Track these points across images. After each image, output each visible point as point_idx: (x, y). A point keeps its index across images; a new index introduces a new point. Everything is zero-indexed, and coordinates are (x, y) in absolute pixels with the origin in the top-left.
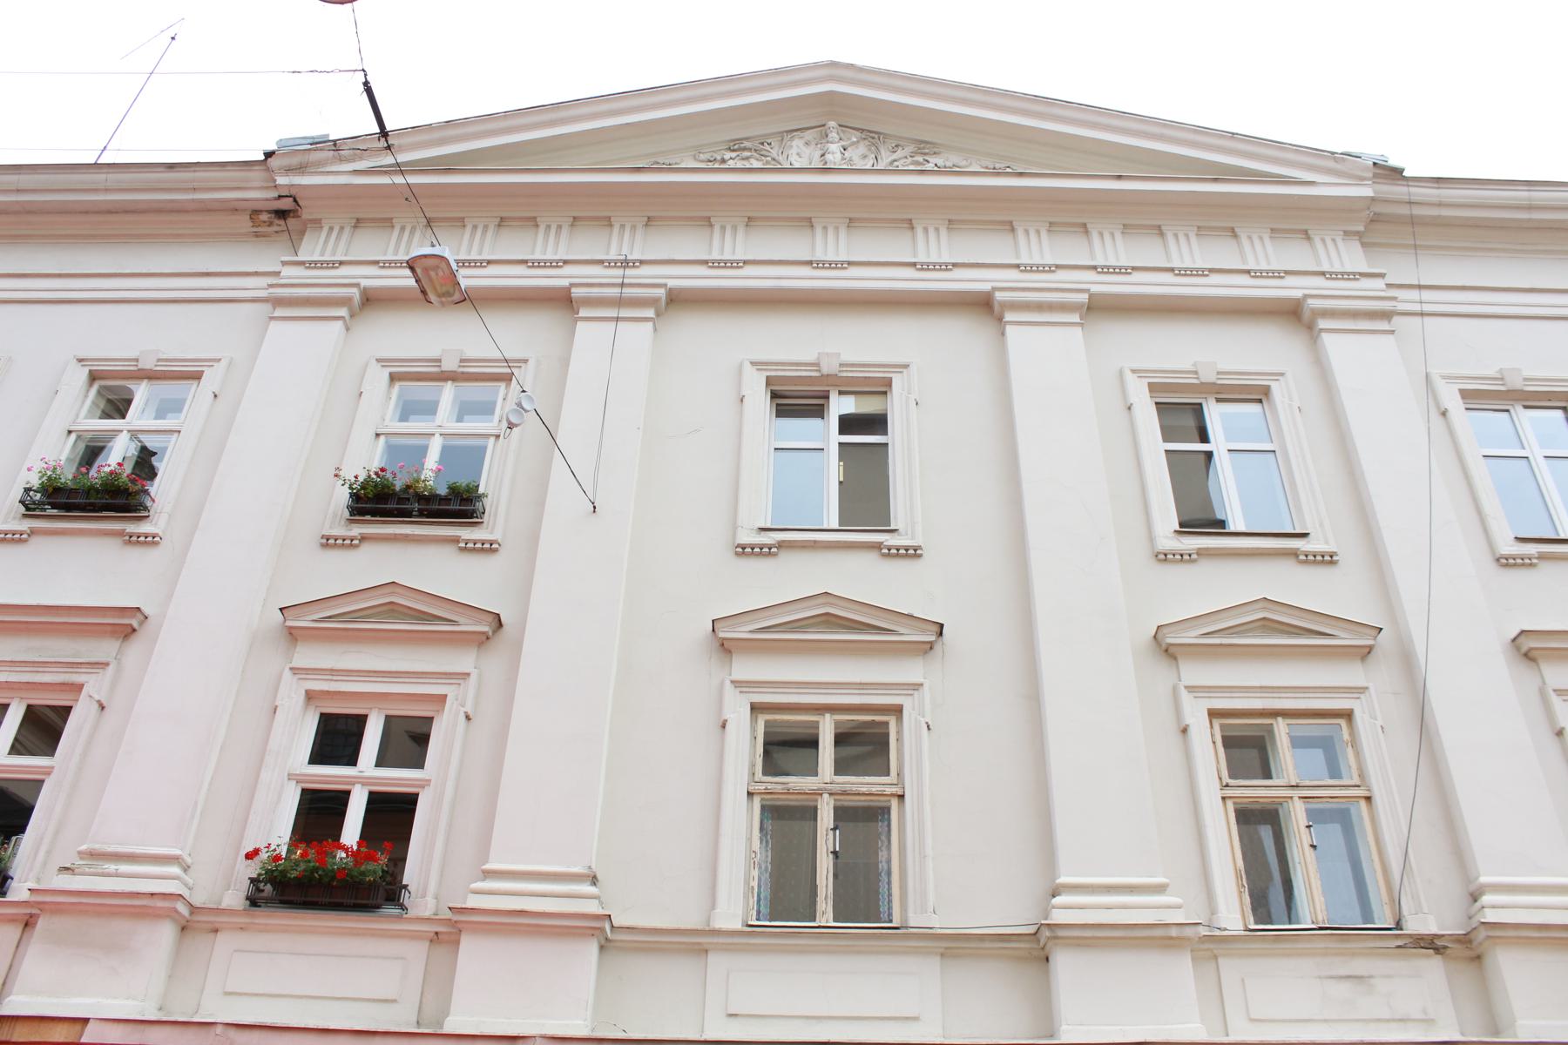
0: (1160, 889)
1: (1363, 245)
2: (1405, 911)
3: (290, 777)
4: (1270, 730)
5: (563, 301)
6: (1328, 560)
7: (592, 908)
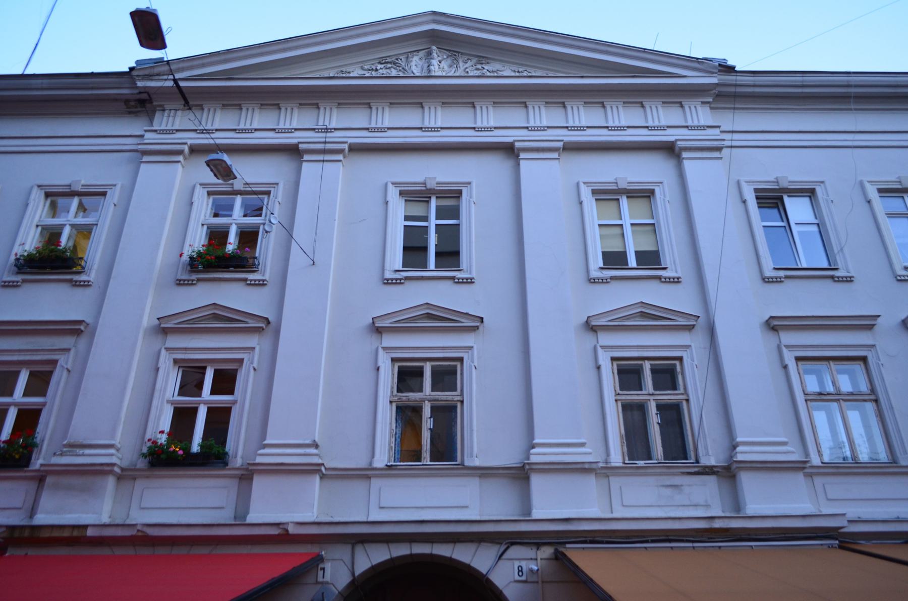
0: (582, 445)
1: (711, 108)
3: (168, 402)
4: (641, 365)
5: (294, 152)
6: (676, 281)
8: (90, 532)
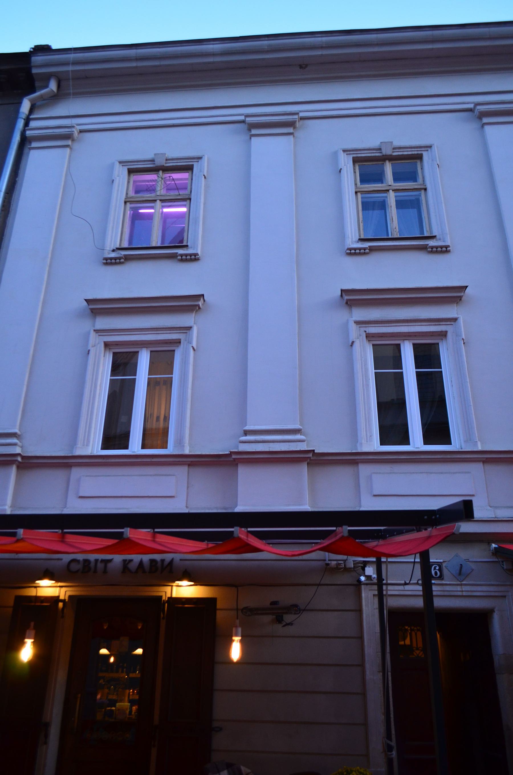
7: (303, 447)
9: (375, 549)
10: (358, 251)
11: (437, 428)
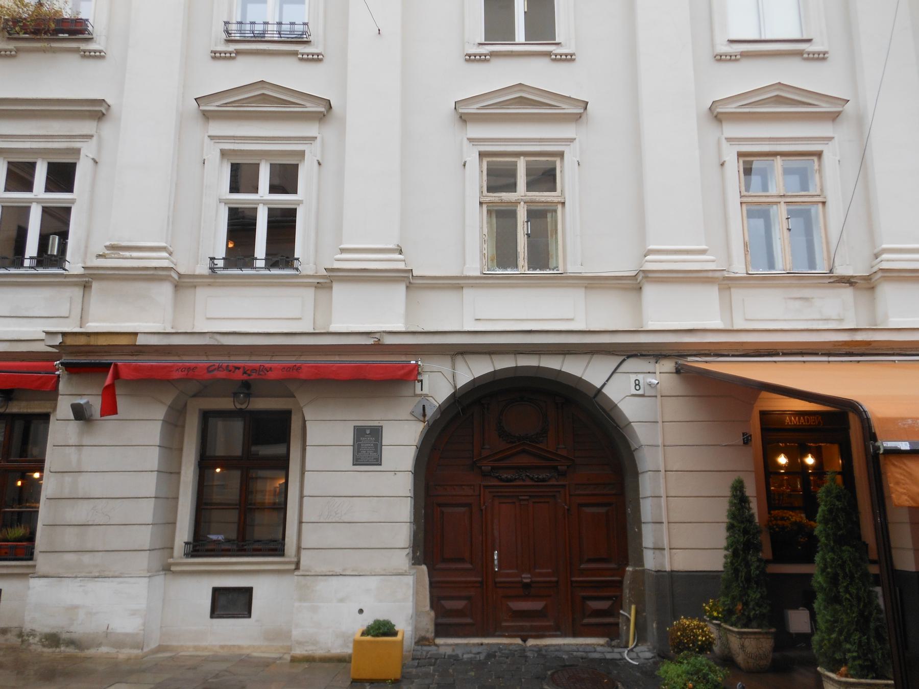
0: (703, 252)
2: (836, 264)
6: (821, 57)
7: (401, 266)
8: (141, 341)
9: (622, 358)
10: (564, 57)
11: (540, 256)
